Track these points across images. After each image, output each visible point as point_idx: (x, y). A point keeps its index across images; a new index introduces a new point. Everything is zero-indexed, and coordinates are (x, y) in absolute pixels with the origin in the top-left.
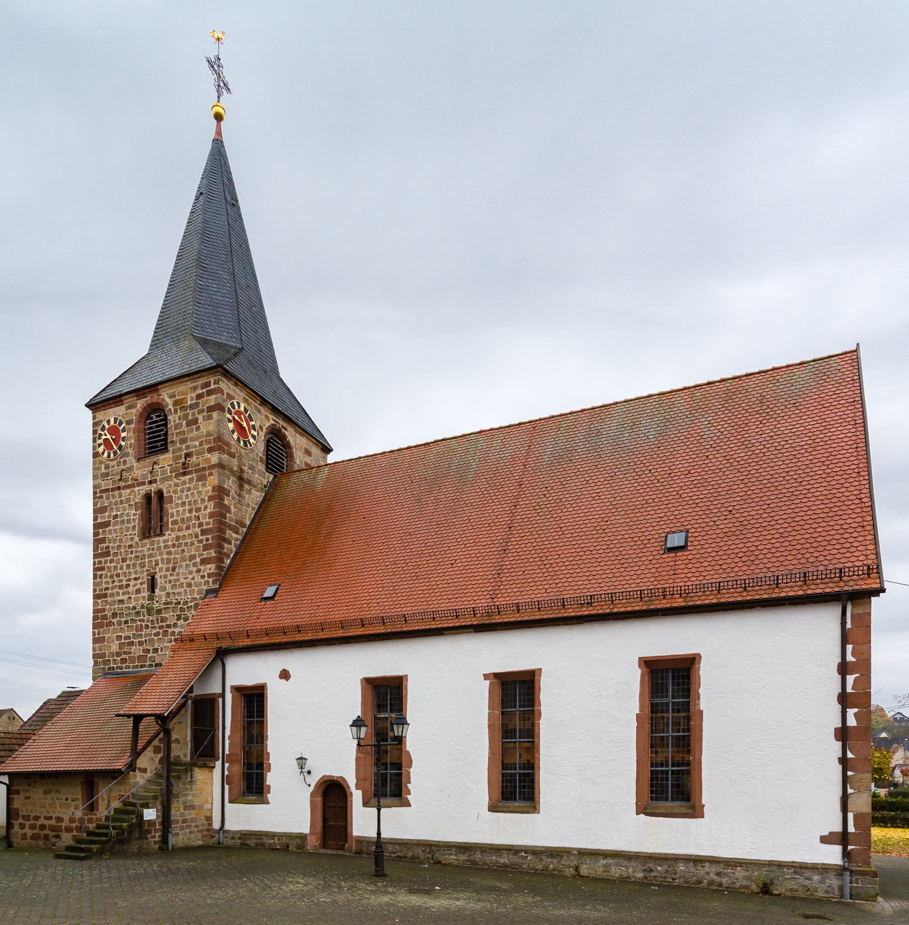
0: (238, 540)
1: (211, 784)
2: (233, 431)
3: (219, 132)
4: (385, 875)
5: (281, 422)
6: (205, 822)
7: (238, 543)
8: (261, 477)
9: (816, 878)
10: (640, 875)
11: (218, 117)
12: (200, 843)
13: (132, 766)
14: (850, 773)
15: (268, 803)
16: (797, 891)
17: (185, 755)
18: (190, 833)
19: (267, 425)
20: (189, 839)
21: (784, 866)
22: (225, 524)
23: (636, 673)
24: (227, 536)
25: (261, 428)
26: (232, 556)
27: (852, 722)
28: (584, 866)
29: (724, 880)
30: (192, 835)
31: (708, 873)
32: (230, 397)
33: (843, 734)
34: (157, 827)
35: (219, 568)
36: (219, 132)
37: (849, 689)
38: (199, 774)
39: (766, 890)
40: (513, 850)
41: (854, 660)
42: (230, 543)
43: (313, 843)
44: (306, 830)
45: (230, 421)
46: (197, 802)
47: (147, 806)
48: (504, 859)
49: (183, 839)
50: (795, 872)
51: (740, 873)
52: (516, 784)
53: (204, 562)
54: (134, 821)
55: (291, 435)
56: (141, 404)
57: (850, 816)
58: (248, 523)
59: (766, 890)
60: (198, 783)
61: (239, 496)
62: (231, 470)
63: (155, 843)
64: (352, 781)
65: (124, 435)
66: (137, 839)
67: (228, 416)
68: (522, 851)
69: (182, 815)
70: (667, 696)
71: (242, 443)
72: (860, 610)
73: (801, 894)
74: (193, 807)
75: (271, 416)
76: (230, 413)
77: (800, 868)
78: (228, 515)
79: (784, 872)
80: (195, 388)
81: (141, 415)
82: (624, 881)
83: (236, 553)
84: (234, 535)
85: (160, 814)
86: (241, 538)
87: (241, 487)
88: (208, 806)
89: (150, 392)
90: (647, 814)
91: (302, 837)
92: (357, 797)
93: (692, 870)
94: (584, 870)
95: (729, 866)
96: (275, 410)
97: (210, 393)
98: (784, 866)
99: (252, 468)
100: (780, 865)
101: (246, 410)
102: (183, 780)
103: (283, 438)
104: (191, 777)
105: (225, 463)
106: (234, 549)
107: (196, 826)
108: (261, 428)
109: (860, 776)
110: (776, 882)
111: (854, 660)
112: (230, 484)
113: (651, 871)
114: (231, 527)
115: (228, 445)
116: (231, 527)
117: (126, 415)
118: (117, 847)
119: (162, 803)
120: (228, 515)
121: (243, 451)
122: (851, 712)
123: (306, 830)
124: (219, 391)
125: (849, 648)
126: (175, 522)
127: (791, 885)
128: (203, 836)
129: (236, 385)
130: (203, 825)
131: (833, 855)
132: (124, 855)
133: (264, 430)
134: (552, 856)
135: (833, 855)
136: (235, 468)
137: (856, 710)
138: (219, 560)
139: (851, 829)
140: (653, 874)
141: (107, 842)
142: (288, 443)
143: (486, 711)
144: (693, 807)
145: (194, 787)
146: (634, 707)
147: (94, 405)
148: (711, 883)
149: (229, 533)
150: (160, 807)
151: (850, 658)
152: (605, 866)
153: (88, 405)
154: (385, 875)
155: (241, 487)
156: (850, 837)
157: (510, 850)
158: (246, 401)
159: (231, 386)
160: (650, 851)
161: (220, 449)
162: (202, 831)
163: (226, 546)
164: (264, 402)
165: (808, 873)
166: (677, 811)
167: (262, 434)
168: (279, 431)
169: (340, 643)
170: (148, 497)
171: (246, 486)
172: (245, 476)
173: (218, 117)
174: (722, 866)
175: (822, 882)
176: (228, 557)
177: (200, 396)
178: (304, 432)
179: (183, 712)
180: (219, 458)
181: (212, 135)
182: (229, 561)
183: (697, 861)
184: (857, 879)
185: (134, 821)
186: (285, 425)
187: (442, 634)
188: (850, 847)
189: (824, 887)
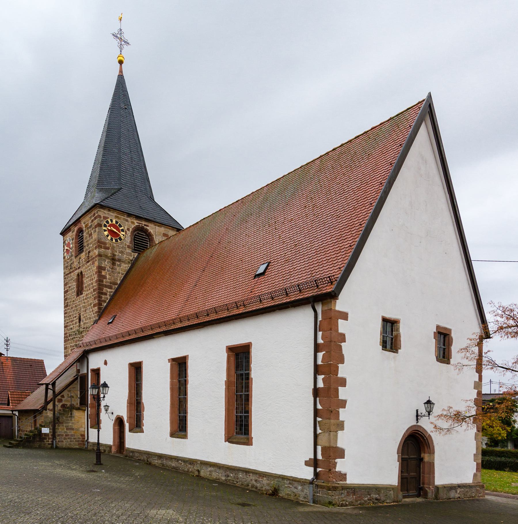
0: (112, 292)
1: (81, 418)
2: (108, 236)
3: (121, 71)
4: (101, 464)
5: (144, 223)
6: (80, 437)
7: (112, 294)
8: (129, 255)
9: (300, 488)
10: (224, 478)
11: (121, 62)
12: (77, 447)
13: (44, 408)
14: (319, 419)
15: (143, 432)
16: (290, 495)
17: (77, 404)
18: (70, 441)
19: (133, 227)
20: (70, 444)
21: (285, 479)
22: (103, 285)
23: (224, 355)
24: (104, 291)
25: (128, 229)
26: (107, 301)
27: (320, 384)
28: (203, 471)
29: (258, 485)
30: (72, 443)
31: (251, 480)
32: (105, 218)
33: (316, 392)
34: (50, 437)
35: (99, 308)
36: (121, 71)
37: (319, 362)
38: (76, 413)
39: (275, 493)
40: (177, 459)
41: (322, 342)
42: (106, 294)
43: (114, 450)
44: (111, 443)
45: (105, 231)
46: (75, 427)
47: (44, 427)
48: (174, 464)
49: (66, 444)
50: (290, 483)
51: (265, 481)
52: (239, 427)
53: (94, 306)
54: (36, 433)
55: (151, 228)
56: (76, 229)
57: (319, 448)
58: (119, 282)
59: (275, 493)
60: (76, 417)
61: (112, 269)
62: (106, 256)
63: (49, 444)
64: (125, 419)
65: (109, 238)
66: (38, 441)
67: (104, 228)
68: (180, 460)
69: (66, 432)
70: (243, 370)
71: (114, 240)
72: (326, 308)
73: (292, 498)
74: (73, 429)
75: (135, 221)
76: (105, 226)
77: (293, 480)
78: (104, 280)
79: (284, 483)
80: (91, 217)
81: (76, 234)
82: (214, 481)
83: (111, 300)
84: (109, 290)
85: (51, 431)
86: (113, 291)
87: (114, 264)
88: (83, 429)
89: (78, 223)
90: (230, 442)
91: (110, 447)
92: (127, 426)
93: (245, 477)
94: (202, 474)
95: (260, 476)
96: (138, 217)
97: (95, 218)
98: (285, 479)
99: (122, 252)
100: (283, 478)
101: (117, 222)
102: (66, 415)
103: (146, 231)
104: (71, 414)
105: (102, 254)
106: (109, 298)
107: (75, 439)
108: (128, 229)
109: (324, 421)
110: (281, 488)
111: (322, 342)
112: (106, 264)
113: (228, 476)
114: (106, 286)
115: (105, 243)
116: (106, 286)
117: (71, 235)
118: (27, 444)
119: (52, 425)
120: (104, 280)
121: (115, 245)
122: (320, 378)
123: (111, 443)
124: (100, 216)
125: (320, 334)
126: (86, 287)
127: (287, 491)
128: (79, 444)
129: (109, 210)
130: (79, 438)
131: (308, 473)
132: (31, 447)
133: (131, 230)
134: (190, 464)
135: (308, 473)
136: (109, 255)
137: (323, 376)
138: (100, 304)
139: (320, 457)
140: (229, 478)
141: (21, 441)
142: (150, 233)
143: (169, 380)
144: (248, 439)
145: (73, 419)
146: (224, 377)
147: (64, 233)
148: (253, 486)
149: (105, 290)
150: (51, 428)
151: (320, 341)
152: (210, 471)
153: (61, 234)
154: (101, 464)
155: (114, 264)
156: (319, 463)
157: (175, 459)
158: (116, 217)
159: (106, 212)
160: (230, 464)
161: (99, 247)
162: (78, 441)
163: (103, 296)
164: (129, 215)
165: (296, 484)
166: (242, 441)
167: (129, 233)
168: (143, 228)
169: (119, 346)
170: (78, 275)
171: (118, 263)
172: (117, 257)
173: (121, 62)
174: (258, 476)
175: (302, 491)
176: (105, 301)
177: (92, 221)
178: (161, 224)
179: (75, 382)
180: (99, 252)
181: (117, 73)
182: (105, 304)
183: (247, 471)
184: (319, 491)
185: (36, 433)
186: (146, 224)
187: (154, 338)
188: (319, 470)
189: (302, 494)
